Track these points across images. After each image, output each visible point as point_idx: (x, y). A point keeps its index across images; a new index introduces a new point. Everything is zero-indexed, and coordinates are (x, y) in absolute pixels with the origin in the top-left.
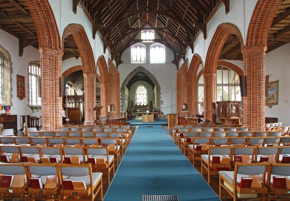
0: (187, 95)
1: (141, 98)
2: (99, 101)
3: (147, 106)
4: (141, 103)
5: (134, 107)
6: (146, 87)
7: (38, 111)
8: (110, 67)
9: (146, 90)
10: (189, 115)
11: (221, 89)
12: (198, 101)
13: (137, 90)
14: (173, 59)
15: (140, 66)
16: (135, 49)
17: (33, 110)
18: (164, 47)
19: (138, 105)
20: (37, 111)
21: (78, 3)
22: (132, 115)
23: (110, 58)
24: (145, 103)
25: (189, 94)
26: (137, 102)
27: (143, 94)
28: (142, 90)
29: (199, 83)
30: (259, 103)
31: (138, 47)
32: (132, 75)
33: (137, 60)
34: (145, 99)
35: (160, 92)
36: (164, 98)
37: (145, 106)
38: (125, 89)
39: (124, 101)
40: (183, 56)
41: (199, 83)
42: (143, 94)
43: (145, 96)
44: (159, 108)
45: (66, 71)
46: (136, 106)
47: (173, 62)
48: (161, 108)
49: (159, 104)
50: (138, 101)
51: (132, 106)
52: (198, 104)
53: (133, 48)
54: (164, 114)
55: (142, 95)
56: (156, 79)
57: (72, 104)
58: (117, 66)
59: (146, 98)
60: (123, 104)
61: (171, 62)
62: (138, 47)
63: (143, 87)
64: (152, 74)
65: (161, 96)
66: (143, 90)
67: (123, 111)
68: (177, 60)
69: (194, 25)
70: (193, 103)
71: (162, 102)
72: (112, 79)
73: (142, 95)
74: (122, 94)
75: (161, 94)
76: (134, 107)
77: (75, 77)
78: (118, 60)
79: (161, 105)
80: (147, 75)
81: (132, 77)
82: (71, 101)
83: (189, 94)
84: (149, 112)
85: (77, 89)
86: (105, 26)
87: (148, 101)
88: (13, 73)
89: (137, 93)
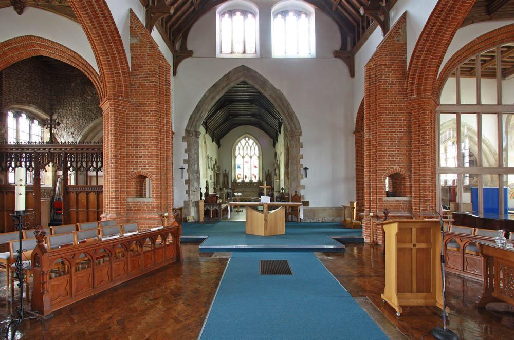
0: (404, 143)
1: (247, 166)
3: (260, 183)
4: (246, 177)
5: (230, 187)
6: (258, 140)
8: (135, 41)
9: (257, 147)
10: (411, 212)
11: (474, 132)
12: (439, 165)
13: (237, 147)
14: (337, 46)
15: (243, 66)
16: (230, 19)
18: (310, 13)
19: (240, 181)
21: (153, 26)
22: (217, 208)
23: (141, 16)
24: (255, 177)
25: (410, 139)
26: (237, 174)
27: (251, 157)
28: (249, 148)
29: (441, 102)
30: (118, 203)
31: (238, 14)
32: (218, 93)
33: (235, 50)
34: (256, 167)
35: (301, 142)
36: (309, 157)
37: (255, 183)
38: (197, 134)
39: (196, 166)
40: (382, 18)
41: (441, 102)
42: (251, 157)
43: (256, 161)
44: (297, 187)
46: (235, 183)
47: (337, 54)
48: (303, 187)
49: (297, 177)
50: (238, 171)
51: (225, 185)
52: (439, 174)
53: (222, 14)
54: (311, 206)
55: (247, 158)
56: (289, 104)
58: (176, 63)
59: (258, 166)
60: (192, 177)
61: (331, 55)
62: (238, 14)
63: (251, 140)
65: (302, 151)
66: (251, 148)
67: (192, 197)
68: (349, 48)
69: (362, 12)
70: (428, 170)
71: (306, 169)
72: (141, 85)
73: (247, 158)
74: (188, 146)
75: (302, 147)
76: (230, 187)
77: (54, 97)
78: (178, 46)
80: (260, 93)
81: (218, 98)
83: (410, 139)
84: (269, 202)
85: (60, 133)
86: (172, 11)
87: (262, 173)
89: (236, 155)
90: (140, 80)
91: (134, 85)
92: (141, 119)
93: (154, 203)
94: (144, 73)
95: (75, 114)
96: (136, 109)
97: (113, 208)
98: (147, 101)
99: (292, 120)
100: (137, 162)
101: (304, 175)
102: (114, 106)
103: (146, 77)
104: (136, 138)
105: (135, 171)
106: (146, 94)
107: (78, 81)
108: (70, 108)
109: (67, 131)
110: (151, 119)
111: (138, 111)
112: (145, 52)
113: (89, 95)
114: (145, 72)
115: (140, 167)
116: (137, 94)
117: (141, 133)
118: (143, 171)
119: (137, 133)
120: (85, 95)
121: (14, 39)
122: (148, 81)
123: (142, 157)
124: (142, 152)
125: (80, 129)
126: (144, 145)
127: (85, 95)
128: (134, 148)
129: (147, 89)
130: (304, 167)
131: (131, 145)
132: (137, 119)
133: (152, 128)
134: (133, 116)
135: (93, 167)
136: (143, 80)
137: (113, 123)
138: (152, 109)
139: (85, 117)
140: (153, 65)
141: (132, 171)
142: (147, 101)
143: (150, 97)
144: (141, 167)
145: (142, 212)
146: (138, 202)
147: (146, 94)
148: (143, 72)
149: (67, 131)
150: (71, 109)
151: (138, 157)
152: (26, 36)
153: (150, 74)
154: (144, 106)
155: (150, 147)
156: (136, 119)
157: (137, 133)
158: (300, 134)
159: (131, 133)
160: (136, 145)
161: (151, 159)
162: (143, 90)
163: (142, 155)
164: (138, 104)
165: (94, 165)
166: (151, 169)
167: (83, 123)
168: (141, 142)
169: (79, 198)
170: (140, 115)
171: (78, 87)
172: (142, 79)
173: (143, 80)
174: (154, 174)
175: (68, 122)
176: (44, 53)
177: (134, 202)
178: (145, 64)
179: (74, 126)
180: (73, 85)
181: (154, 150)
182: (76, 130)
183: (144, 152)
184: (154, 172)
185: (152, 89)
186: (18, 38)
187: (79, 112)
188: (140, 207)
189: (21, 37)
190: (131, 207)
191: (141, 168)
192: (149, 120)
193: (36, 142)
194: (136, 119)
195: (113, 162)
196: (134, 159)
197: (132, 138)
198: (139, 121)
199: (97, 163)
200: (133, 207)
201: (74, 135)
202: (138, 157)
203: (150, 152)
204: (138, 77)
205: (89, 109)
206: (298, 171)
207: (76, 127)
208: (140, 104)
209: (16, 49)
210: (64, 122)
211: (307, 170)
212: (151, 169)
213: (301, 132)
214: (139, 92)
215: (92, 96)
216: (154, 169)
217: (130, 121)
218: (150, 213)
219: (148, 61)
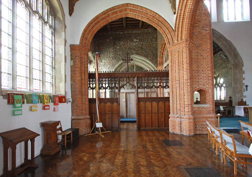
2: (160, 83)
7: (33, 108)
17: (15, 107)
20: (31, 110)
35: (243, 70)
44: (241, 96)
45: (97, 17)
48: (245, 97)
56: (235, 49)
57: (92, 90)
64: (228, 39)
65: (244, 76)
71: (247, 86)
72: (200, 33)
75: (244, 73)
79: (244, 93)
82: (115, 84)
88: (58, 123)
90: (199, 30)
91: (196, 33)
92: (201, 54)
93: (211, 107)
94: (202, 25)
95: (110, 57)
96: (197, 48)
97: (190, 111)
98: (204, 43)
99: (236, 58)
100: (199, 81)
101: (246, 90)
102: (188, 46)
103: (202, 28)
104: (197, 66)
105: (198, 87)
106: (203, 39)
107: (111, 38)
108: (106, 54)
109: (105, 67)
110: (207, 54)
111: (199, 49)
112: (201, 12)
113: (118, 46)
114: (202, 25)
115: (201, 84)
116: (198, 39)
117: (201, 63)
118: (203, 87)
119: (198, 63)
120: (116, 46)
121: (118, 6)
122: (205, 30)
123: (202, 78)
124: (201, 75)
125: (113, 65)
126: (203, 70)
127: (116, 46)
128: (196, 73)
129: (204, 35)
130: (245, 85)
131: (195, 71)
132: (198, 54)
133: (208, 60)
134: (195, 52)
135: (103, 87)
136: (201, 30)
137: (188, 57)
138: (208, 47)
139: (116, 59)
140: (207, 20)
141: (196, 88)
142: (204, 43)
143: (206, 40)
144: (202, 84)
145: (203, 113)
146: (200, 107)
147: (203, 39)
148: (201, 25)
149: (105, 67)
150: (107, 54)
151: (199, 78)
152: (125, 4)
153: (205, 26)
154: (202, 46)
155: (207, 72)
156: (197, 54)
157: (198, 63)
158: (243, 66)
159: (194, 63)
160: (198, 71)
161: (208, 80)
162: (201, 36)
163: (202, 77)
164: (198, 45)
165: (91, 86)
166: (208, 86)
167: (115, 62)
168: (201, 69)
169: (146, 105)
170: (200, 52)
171: (111, 41)
172: (200, 29)
173: (201, 30)
174: (209, 89)
175: (105, 62)
176: (131, 15)
177: (197, 107)
178: (202, 20)
179: (109, 63)
180: (108, 40)
181: (210, 73)
182: (111, 66)
183: (203, 75)
184: (210, 87)
185: (207, 35)
186: (120, 5)
187: (112, 56)
188: (201, 110)
189: (122, 4)
190: (195, 110)
191: (201, 85)
192: (206, 55)
193: (92, 72)
194: (197, 54)
195: (188, 81)
196: (197, 80)
197: (195, 66)
198: (199, 55)
199: (93, 84)
200: (197, 110)
201: (110, 69)
202: (199, 78)
203: (207, 75)
204: (198, 28)
205: (118, 54)
206: (241, 87)
207: (111, 64)
208: (199, 45)
209: (116, 13)
210: (103, 62)
211: (248, 87)
212: (208, 86)
213: (243, 65)
214: (198, 37)
215: (120, 47)
216: (211, 86)
217: (194, 56)
218: (208, 114)
219: (204, 18)
